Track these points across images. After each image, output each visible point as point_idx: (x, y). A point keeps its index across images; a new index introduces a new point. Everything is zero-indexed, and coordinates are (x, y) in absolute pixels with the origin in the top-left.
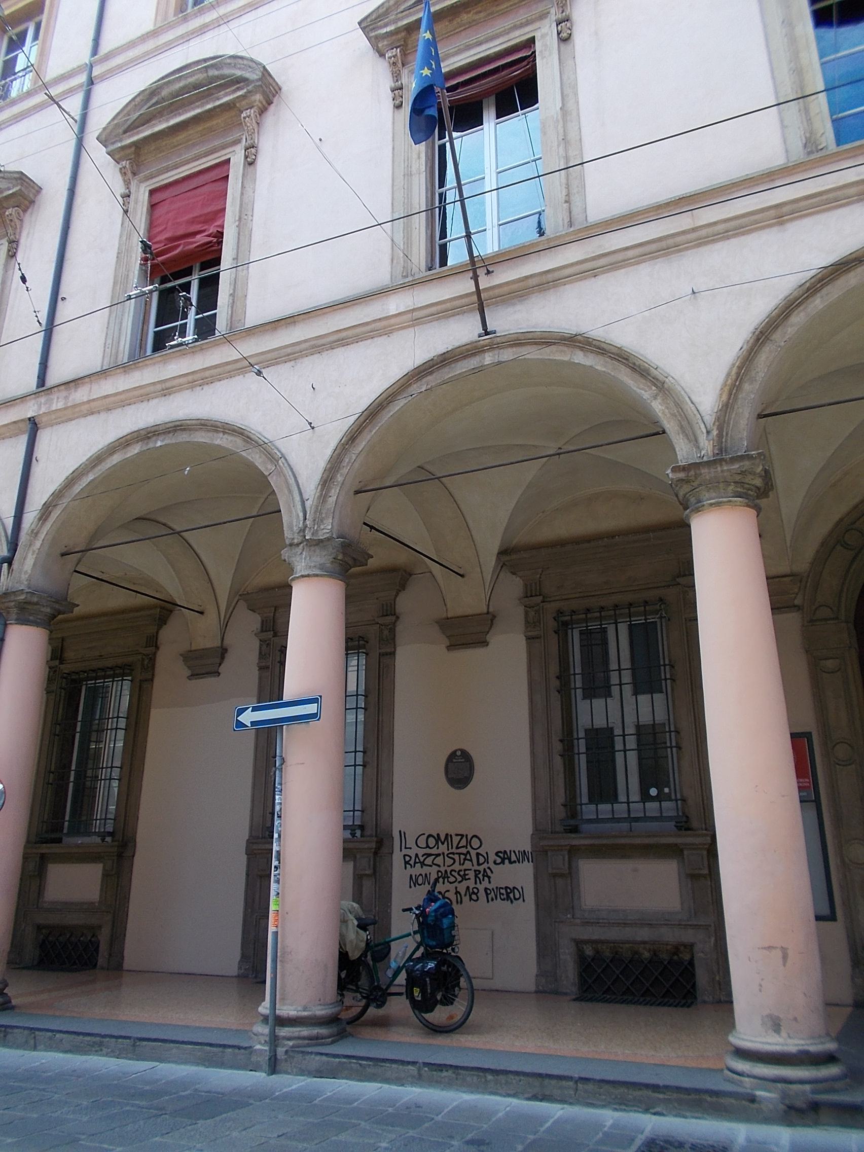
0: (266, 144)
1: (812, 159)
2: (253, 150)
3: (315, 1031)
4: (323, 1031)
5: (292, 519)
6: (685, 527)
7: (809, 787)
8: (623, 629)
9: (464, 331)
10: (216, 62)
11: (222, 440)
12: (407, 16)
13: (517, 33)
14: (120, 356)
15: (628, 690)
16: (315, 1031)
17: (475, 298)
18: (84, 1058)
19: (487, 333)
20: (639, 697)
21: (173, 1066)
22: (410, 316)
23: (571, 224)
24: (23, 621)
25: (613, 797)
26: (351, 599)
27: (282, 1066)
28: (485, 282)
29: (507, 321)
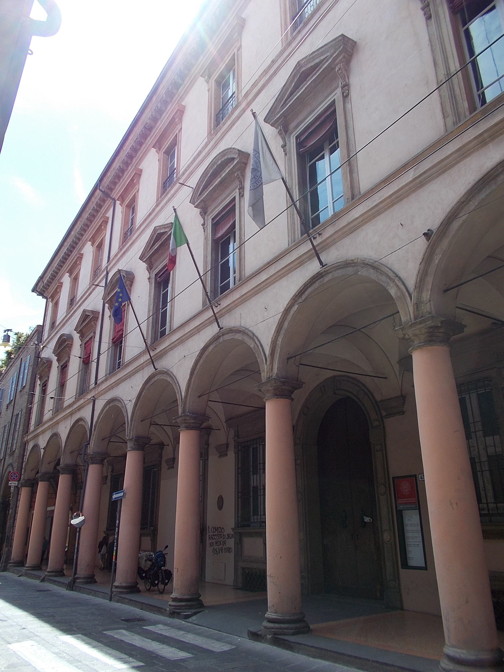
0: (355, 81)
1: (295, 245)
2: (346, 87)
3: (121, 590)
4: (125, 590)
5: (407, 312)
6: (411, 357)
7: (416, 502)
8: (474, 396)
9: (314, 267)
10: (224, 153)
11: (238, 336)
12: (283, 109)
13: (217, 209)
14: (296, 237)
15: (480, 434)
16: (121, 590)
17: (313, 251)
18: (58, 587)
19: (221, 329)
20: (486, 438)
21: (86, 595)
22: (389, 200)
23: (446, 131)
24: (93, 463)
25: (257, 515)
26: (455, 358)
27: (113, 599)
28: (152, 354)
29: (331, 257)
